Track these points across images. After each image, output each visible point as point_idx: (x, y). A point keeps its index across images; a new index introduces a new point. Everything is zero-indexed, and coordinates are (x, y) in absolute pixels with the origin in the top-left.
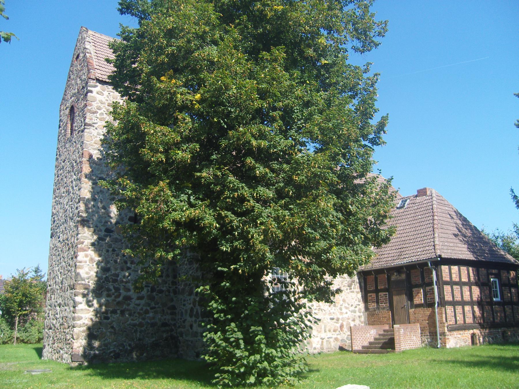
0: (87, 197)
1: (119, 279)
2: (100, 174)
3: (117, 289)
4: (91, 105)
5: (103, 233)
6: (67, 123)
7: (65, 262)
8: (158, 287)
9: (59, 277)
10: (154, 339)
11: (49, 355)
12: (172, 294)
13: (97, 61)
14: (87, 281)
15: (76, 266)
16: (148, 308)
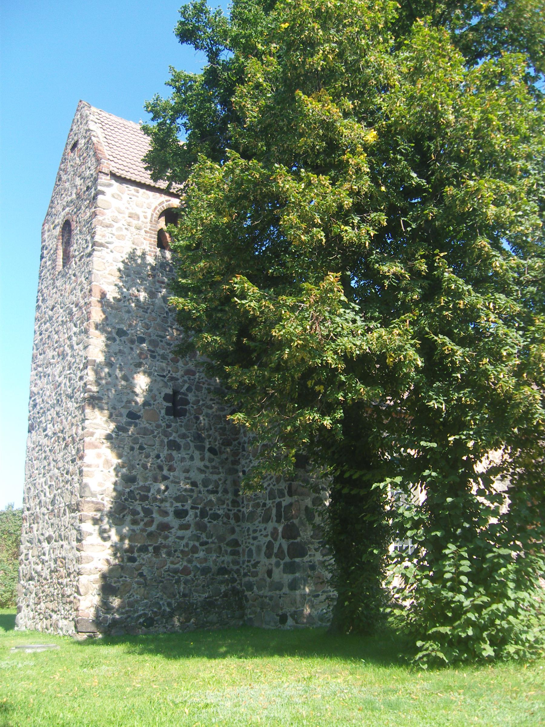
0: (98, 361)
1: (150, 494)
2: (118, 323)
3: (148, 512)
4: (103, 214)
5: (124, 420)
6: (56, 249)
7: (59, 469)
8: (211, 509)
9: (48, 494)
10: (207, 595)
11: (29, 623)
12: (232, 522)
13: (108, 149)
14: (100, 497)
15: (81, 472)
16: (197, 544)
